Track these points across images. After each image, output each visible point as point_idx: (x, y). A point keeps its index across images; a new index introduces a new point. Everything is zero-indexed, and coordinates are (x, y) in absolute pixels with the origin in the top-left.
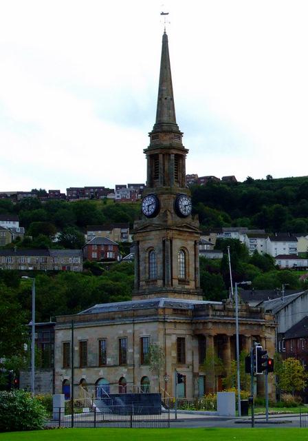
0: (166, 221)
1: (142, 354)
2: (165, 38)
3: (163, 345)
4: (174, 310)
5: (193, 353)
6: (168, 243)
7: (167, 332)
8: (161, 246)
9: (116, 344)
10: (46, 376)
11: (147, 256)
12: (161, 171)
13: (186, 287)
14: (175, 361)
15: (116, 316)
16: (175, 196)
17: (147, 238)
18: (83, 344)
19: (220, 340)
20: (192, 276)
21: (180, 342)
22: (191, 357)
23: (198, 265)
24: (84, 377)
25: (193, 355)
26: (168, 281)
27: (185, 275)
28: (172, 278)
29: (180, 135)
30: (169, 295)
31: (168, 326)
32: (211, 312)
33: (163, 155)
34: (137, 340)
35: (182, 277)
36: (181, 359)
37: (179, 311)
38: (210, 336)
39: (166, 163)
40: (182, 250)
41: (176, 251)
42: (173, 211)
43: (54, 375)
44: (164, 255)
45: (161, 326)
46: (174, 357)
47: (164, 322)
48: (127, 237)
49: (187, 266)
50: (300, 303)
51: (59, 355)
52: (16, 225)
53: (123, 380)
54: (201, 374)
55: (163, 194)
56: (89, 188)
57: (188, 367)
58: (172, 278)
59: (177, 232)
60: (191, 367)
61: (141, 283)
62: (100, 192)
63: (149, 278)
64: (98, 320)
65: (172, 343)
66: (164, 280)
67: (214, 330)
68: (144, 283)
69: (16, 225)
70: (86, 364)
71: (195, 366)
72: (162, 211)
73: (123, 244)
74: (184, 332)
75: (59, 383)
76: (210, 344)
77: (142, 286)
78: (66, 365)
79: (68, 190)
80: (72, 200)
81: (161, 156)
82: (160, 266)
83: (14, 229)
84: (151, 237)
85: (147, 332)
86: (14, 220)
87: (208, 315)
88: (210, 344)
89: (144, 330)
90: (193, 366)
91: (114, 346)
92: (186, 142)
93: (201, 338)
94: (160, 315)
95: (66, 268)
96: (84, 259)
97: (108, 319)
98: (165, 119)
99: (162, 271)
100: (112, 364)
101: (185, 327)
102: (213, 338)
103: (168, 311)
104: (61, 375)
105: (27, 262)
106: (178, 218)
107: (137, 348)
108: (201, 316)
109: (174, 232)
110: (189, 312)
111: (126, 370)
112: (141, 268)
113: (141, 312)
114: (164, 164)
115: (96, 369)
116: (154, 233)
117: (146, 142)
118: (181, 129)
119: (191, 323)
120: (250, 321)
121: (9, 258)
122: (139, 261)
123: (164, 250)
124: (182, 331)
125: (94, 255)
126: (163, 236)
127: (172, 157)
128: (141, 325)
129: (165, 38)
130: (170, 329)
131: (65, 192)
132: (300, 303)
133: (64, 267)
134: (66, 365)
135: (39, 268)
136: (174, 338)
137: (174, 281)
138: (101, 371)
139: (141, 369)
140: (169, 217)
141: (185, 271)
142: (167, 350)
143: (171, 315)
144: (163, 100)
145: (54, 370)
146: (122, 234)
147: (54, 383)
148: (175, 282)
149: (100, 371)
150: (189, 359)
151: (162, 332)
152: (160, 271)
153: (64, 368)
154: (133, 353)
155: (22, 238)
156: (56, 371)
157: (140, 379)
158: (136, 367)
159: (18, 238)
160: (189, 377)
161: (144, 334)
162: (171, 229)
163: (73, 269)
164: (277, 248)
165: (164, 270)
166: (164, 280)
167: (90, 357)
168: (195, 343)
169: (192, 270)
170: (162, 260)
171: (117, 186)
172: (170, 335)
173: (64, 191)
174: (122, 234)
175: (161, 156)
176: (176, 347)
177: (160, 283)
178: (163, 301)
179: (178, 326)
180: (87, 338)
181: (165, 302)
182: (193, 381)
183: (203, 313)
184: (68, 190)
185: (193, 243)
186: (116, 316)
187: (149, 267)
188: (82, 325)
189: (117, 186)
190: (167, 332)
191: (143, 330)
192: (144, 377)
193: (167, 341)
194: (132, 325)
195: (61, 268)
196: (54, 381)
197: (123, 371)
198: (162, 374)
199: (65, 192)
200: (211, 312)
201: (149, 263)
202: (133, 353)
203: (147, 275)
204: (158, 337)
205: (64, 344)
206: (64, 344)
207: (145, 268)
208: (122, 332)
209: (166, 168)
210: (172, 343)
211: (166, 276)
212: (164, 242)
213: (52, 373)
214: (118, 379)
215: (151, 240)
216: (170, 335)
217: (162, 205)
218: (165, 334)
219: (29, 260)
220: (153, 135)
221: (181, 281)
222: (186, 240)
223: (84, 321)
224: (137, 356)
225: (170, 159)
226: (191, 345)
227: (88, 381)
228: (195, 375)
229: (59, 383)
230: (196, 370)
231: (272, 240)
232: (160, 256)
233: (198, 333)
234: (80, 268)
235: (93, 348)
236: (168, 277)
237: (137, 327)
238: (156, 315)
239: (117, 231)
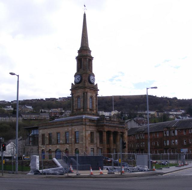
0: (85, 85)
1: (76, 139)
2: (85, 15)
3: (85, 135)
4: (90, 120)
5: (97, 138)
6: (86, 94)
7: (87, 129)
8: (83, 95)
9: (64, 135)
10: (35, 148)
11: (77, 99)
12: (83, 65)
13: (93, 112)
14: (90, 142)
15: (64, 123)
16: (88, 75)
17: (77, 92)
18: (50, 135)
19: (108, 133)
20: (95, 108)
21: (92, 133)
22: (97, 140)
23: (97, 104)
24: (51, 148)
25: (97, 140)
26: (85, 109)
27: (92, 107)
28: (87, 108)
29: (90, 51)
30: (89, 115)
31: (87, 127)
32: (105, 121)
33: (84, 59)
34: (73, 133)
35: (91, 108)
36: (92, 141)
37: (91, 121)
38: (105, 131)
39: (85, 62)
40: (91, 97)
41: (89, 98)
42: (87, 81)
43: (38, 148)
44: (84, 99)
45: (84, 127)
46: (89, 140)
47: (85, 125)
48: (62, 111)
49: (93, 104)
50: (129, 123)
51: (40, 139)
52: (31, 107)
53: (67, 150)
54: (100, 148)
55: (83, 74)
56: (52, 98)
57: (95, 145)
58: (87, 108)
59: (89, 90)
60: (96, 144)
61: (74, 110)
62: (54, 99)
63: (77, 108)
64: (57, 125)
65: (89, 135)
66: (84, 109)
67: (106, 129)
68: (75, 110)
69: (31, 107)
70: (51, 143)
71: (98, 144)
72: (83, 81)
73: (61, 112)
74: (93, 130)
75: (40, 151)
76: (105, 134)
77: (75, 112)
78: (43, 144)
79: (46, 99)
80: (47, 101)
81: (83, 59)
82: (82, 103)
83: (30, 108)
84: (78, 92)
85: (78, 129)
86: (30, 106)
87: (104, 122)
88: (105, 134)
89: (76, 128)
90: (97, 144)
91: (63, 135)
92: (92, 54)
93: (101, 133)
94: (84, 122)
95: (45, 119)
96: (50, 116)
97: (61, 124)
98: (84, 45)
99: (83, 105)
100: (62, 143)
101: (94, 127)
102: (106, 132)
103: (87, 120)
104: (41, 148)
105: (34, 116)
106: (90, 84)
107: (73, 136)
108: (101, 123)
109: (88, 89)
110: (96, 122)
111: (68, 146)
112: (74, 105)
113: (75, 121)
114: (84, 63)
115: (55, 145)
116: (79, 90)
117: (77, 55)
118: (91, 49)
119: (96, 126)
120: (120, 126)
121: (28, 115)
122: (73, 102)
123: (84, 97)
124: (93, 129)
125: (53, 115)
126: (83, 91)
127: (87, 60)
128: (75, 127)
129: (85, 15)
130: (88, 128)
131: (45, 100)
132: (129, 123)
133: (44, 118)
134: (43, 144)
135: (37, 119)
136: (89, 132)
137: (88, 109)
138: (58, 146)
139: (75, 145)
140: (86, 83)
141: (92, 106)
142: (87, 137)
143: (88, 122)
144: (84, 38)
145: (38, 146)
146: (61, 110)
147: (38, 151)
148: (88, 110)
149: (57, 146)
150: (95, 141)
151: (84, 129)
152: (82, 105)
153: (42, 145)
154: (71, 138)
155: (32, 111)
156: (39, 146)
157: (75, 149)
158: (73, 144)
159: (31, 111)
160: (95, 149)
161: (77, 130)
162: (87, 88)
163: (47, 119)
164: (107, 114)
165: (84, 105)
166: (84, 109)
167: (53, 140)
168: (98, 134)
169: (95, 106)
170: (83, 101)
171: (59, 98)
172: (88, 130)
173: (44, 99)
174: (61, 110)
175: (83, 59)
176: (90, 136)
177: (82, 110)
178: (84, 116)
179: (91, 126)
180: (52, 132)
181: (85, 117)
182: (97, 151)
183: (102, 122)
184: (46, 99)
185: (95, 95)
186: (64, 123)
187: (77, 104)
188: (50, 127)
189: (59, 98)
190: (87, 129)
191: (76, 128)
192: (76, 149)
193: (86, 133)
194: (71, 127)
195: (43, 119)
196: (38, 150)
197: (67, 146)
198: (84, 147)
199: (45, 100)
200: (105, 121)
201: (77, 102)
202: (71, 138)
203: (77, 107)
204: (83, 131)
205: (43, 135)
206: (43, 135)
207: (76, 104)
208: (66, 129)
209: (85, 64)
210: (89, 135)
211: (85, 108)
212: (84, 93)
213: (37, 147)
214: (65, 149)
215: (79, 93)
216: (88, 130)
217: (83, 78)
218: (86, 130)
219: (34, 116)
220: (79, 52)
221: (91, 110)
222: (93, 93)
223: (51, 125)
224: (73, 140)
225: (86, 61)
226: (97, 135)
227: (52, 150)
228: (98, 148)
229: (40, 151)
230: (98, 146)
231: (104, 112)
232: (82, 99)
233: (99, 130)
234: (49, 119)
235: (54, 136)
236: (85, 108)
237: (73, 127)
238: (82, 122)
239: (59, 109)
